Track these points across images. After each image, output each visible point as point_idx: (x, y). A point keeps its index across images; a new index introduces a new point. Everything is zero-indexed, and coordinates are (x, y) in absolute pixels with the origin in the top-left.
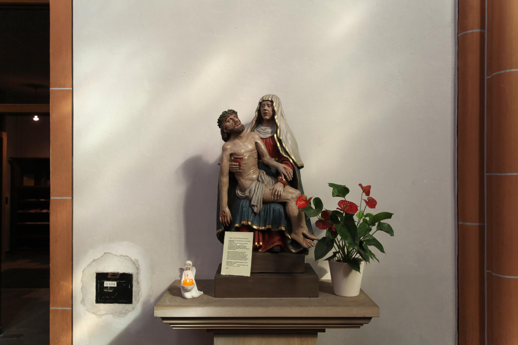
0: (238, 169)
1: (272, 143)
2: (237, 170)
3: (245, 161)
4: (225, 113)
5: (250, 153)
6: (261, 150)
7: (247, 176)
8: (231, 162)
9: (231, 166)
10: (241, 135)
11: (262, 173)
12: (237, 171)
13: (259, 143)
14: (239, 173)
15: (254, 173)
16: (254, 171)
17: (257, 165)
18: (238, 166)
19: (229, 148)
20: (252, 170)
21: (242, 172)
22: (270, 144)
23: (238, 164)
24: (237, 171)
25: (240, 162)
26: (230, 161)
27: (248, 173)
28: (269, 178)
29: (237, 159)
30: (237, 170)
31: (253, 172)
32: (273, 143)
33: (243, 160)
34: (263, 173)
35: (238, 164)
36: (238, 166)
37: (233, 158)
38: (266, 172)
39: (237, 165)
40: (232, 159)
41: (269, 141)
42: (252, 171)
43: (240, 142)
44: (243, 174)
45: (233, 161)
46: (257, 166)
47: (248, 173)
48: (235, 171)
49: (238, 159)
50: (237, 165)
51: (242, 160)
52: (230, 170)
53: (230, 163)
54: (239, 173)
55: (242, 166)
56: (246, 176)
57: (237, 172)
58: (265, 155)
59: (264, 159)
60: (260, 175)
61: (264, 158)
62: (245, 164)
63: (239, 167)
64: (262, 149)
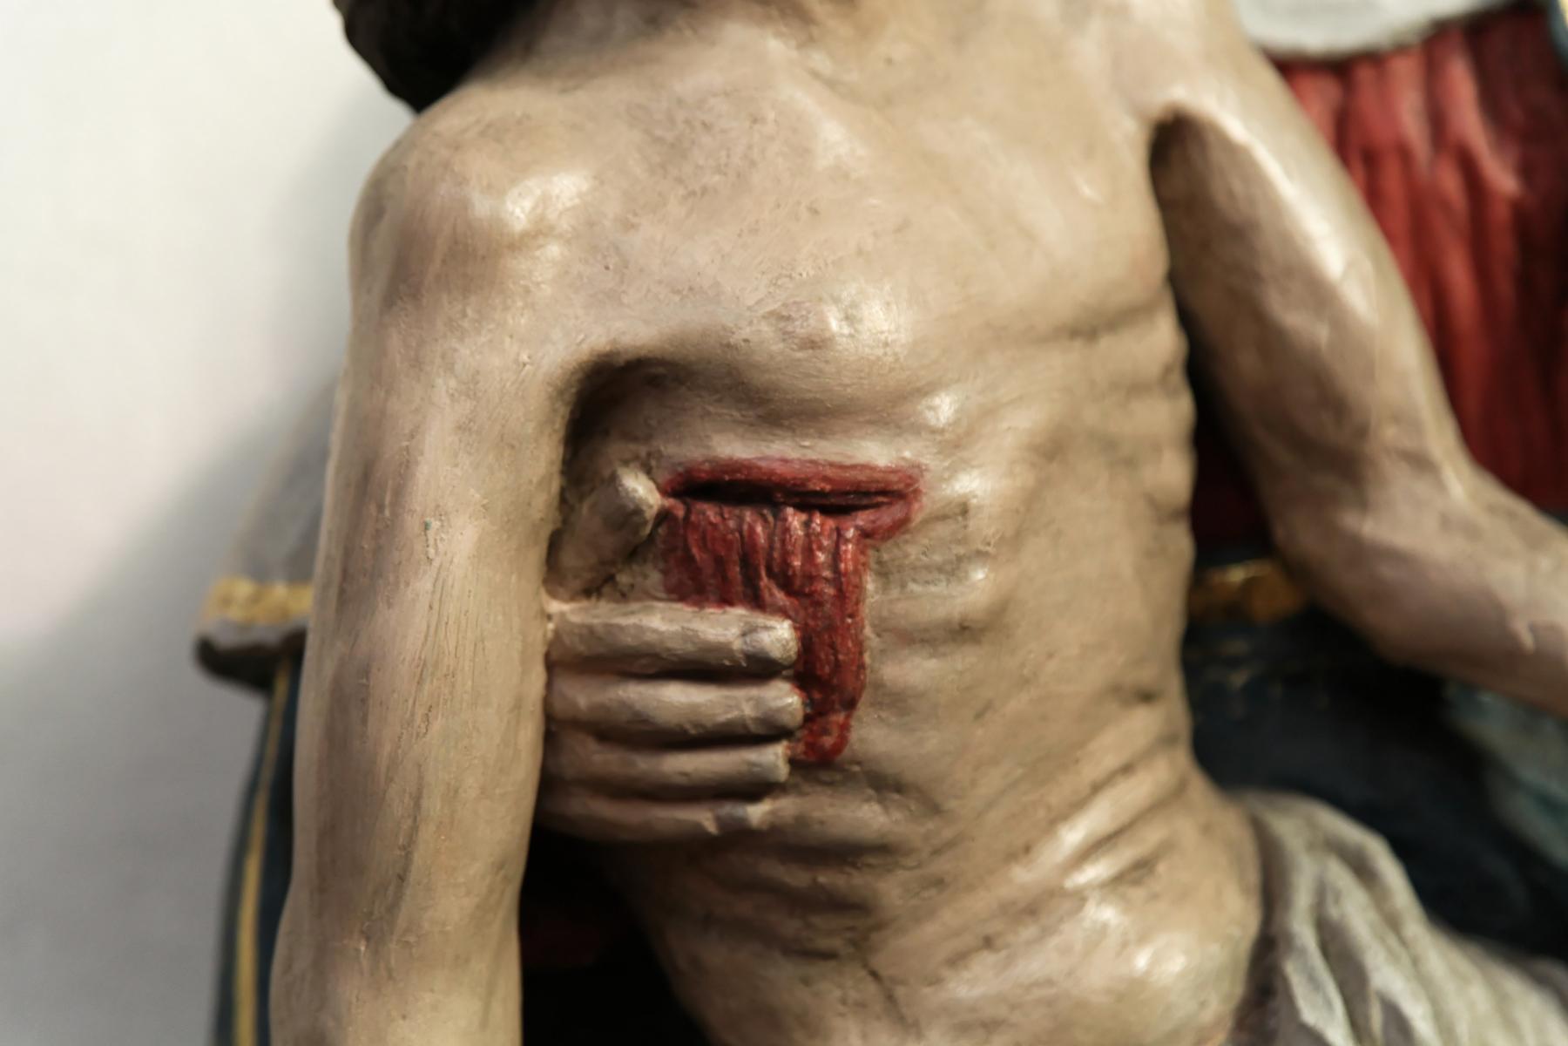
0: (774, 758)
1: (1503, 178)
2: (756, 788)
3: (954, 569)
4: (502, 873)
5: (1059, 363)
6: (1294, 318)
7: (988, 943)
8: (595, 587)
9: (584, 696)
10: (630, 489)
11: (1340, 875)
12: (757, 813)
13: (1234, 151)
14: (796, 877)
15: (1140, 870)
16: (1151, 836)
17: (1174, 684)
18: (784, 699)
19: (540, 231)
20: (1077, 805)
21: (883, 851)
22: (1450, 183)
23: (779, 636)
24: (757, 813)
25: (846, 593)
26: (554, 545)
27: (1025, 876)
28: (1502, 1002)
29: (755, 523)
30: (756, 788)
31: (1125, 855)
32: (1526, 171)
33: (912, 550)
34: (1363, 871)
35: (779, 636)
36: (784, 699)
37: (641, 489)
38: (1402, 850)
39: (759, 669)
40: (627, 515)
41: (1437, 119)
42: (1073, 835)
43: (804, 99)
44: (890, 889)
45: (633, 553)
46: (1171, 713)
47: (1025, 876)
48: (705, 818)
49: (795, 520)
50: (759, 669)
51: (900, 526)
52: (549, 784)
53: (565, 609)
54: (796, 877)
55: (898, 702)
56: (958, 960)
57: (739, 837)
58: (1390, 434)
59: (1371, 528)
60: (1303, 932)
61: (1364, 505)
62: (963, 632)
63: (815, 714)
64: (1320, 294)
